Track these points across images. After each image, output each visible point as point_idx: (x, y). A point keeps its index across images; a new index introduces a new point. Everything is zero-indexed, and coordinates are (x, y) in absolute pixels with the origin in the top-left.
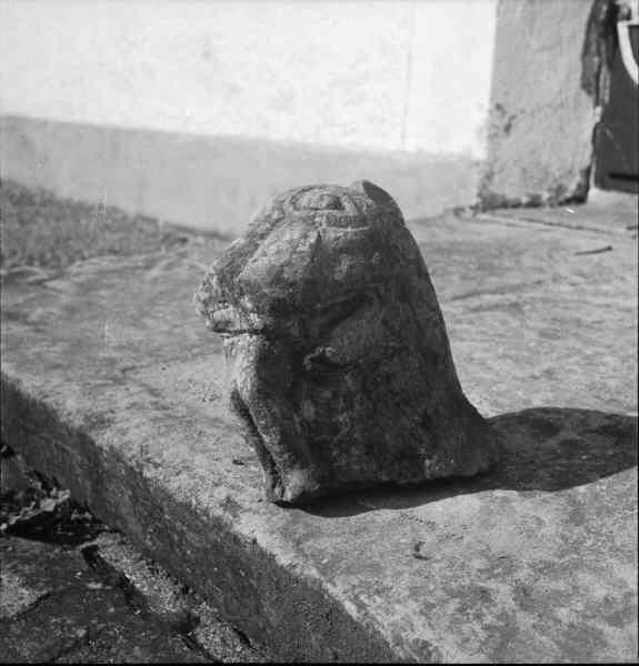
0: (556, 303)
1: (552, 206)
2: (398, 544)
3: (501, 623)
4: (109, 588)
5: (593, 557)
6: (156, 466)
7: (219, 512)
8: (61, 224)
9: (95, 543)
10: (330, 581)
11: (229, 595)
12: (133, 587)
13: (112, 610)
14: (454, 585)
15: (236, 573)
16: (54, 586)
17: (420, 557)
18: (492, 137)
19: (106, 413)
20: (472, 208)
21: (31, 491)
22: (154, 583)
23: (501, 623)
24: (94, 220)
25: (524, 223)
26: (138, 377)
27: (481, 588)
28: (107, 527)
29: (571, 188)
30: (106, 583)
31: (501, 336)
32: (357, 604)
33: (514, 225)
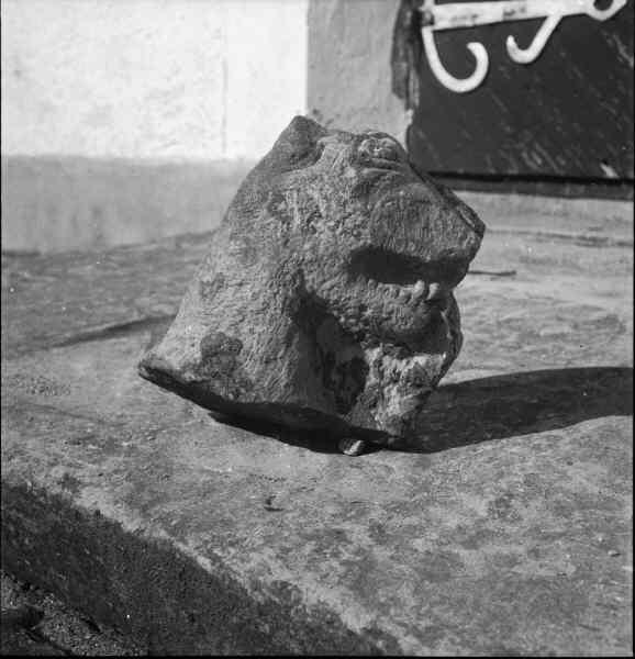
2: (248, 500)
5: (443, 494)
7: (57, 490)
14: (309, 530)
15: (80, 554)
17: (271, 510)
23: (358, 558)
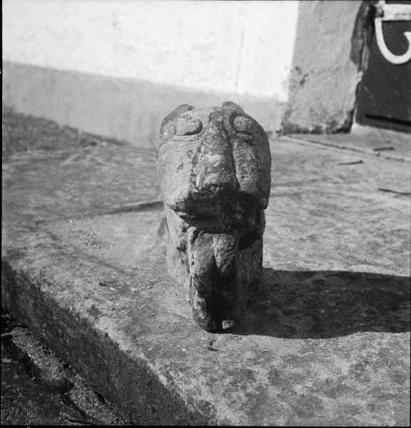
0: (322, 194)
1: (328, 133)
3: (257, 393)
4: (16, 362)
7: (86, 315)
9: (11, 334)
13: (16, 376)
14: (231, 368)
15: (96, 356)
17: (212, 350)
18: (292, 88)
19: (22, 249)
20: (277, 132)
22: (46, 361)
23: (257, 393)
24: (37, 325)
25: (309, 144)
26: (46, 227)
27: (249, 370)
28: (19, 324)
29: (341, 122)
32: (167, 377)
33: (303, 144)
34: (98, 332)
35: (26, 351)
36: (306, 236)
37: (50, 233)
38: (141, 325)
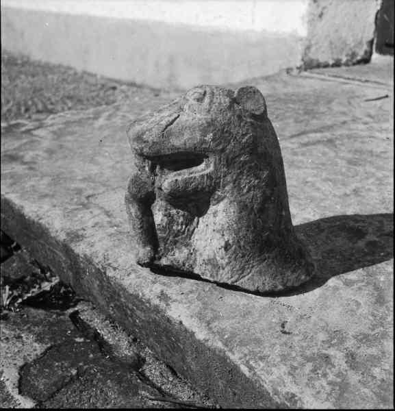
3: (339, 380)
6: (115, 269)
7: (156, 302)
8: (36, 79)
10: (231, 350)
11: (164, 349)
12: (103, 339)
13: (91, 356)
14: (308, 353)
16: (55, 341)
17: (285, 333)
18: (311, 22)
20: (298, 68)
21: (34, 275)
23: (339, 380)
24: (103, 303)
27: (325, 354)
29: (361, 54)
30: (86, 337)
31: (323, 164)
32: (248, 367)
34: (171, 319)
35: (94, 327)
36: (350, 190)
37: (102, 208)
38: (212, 310)
